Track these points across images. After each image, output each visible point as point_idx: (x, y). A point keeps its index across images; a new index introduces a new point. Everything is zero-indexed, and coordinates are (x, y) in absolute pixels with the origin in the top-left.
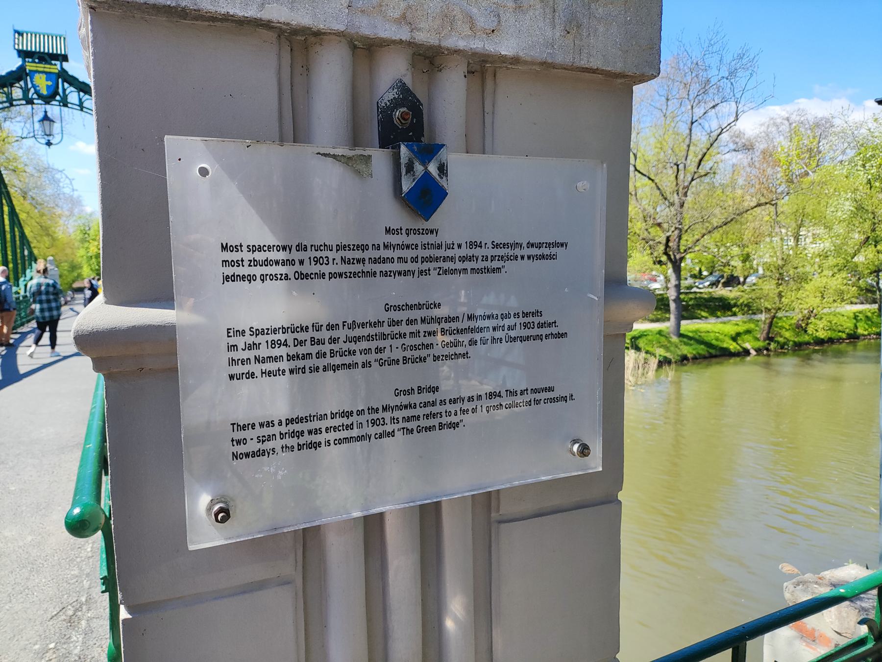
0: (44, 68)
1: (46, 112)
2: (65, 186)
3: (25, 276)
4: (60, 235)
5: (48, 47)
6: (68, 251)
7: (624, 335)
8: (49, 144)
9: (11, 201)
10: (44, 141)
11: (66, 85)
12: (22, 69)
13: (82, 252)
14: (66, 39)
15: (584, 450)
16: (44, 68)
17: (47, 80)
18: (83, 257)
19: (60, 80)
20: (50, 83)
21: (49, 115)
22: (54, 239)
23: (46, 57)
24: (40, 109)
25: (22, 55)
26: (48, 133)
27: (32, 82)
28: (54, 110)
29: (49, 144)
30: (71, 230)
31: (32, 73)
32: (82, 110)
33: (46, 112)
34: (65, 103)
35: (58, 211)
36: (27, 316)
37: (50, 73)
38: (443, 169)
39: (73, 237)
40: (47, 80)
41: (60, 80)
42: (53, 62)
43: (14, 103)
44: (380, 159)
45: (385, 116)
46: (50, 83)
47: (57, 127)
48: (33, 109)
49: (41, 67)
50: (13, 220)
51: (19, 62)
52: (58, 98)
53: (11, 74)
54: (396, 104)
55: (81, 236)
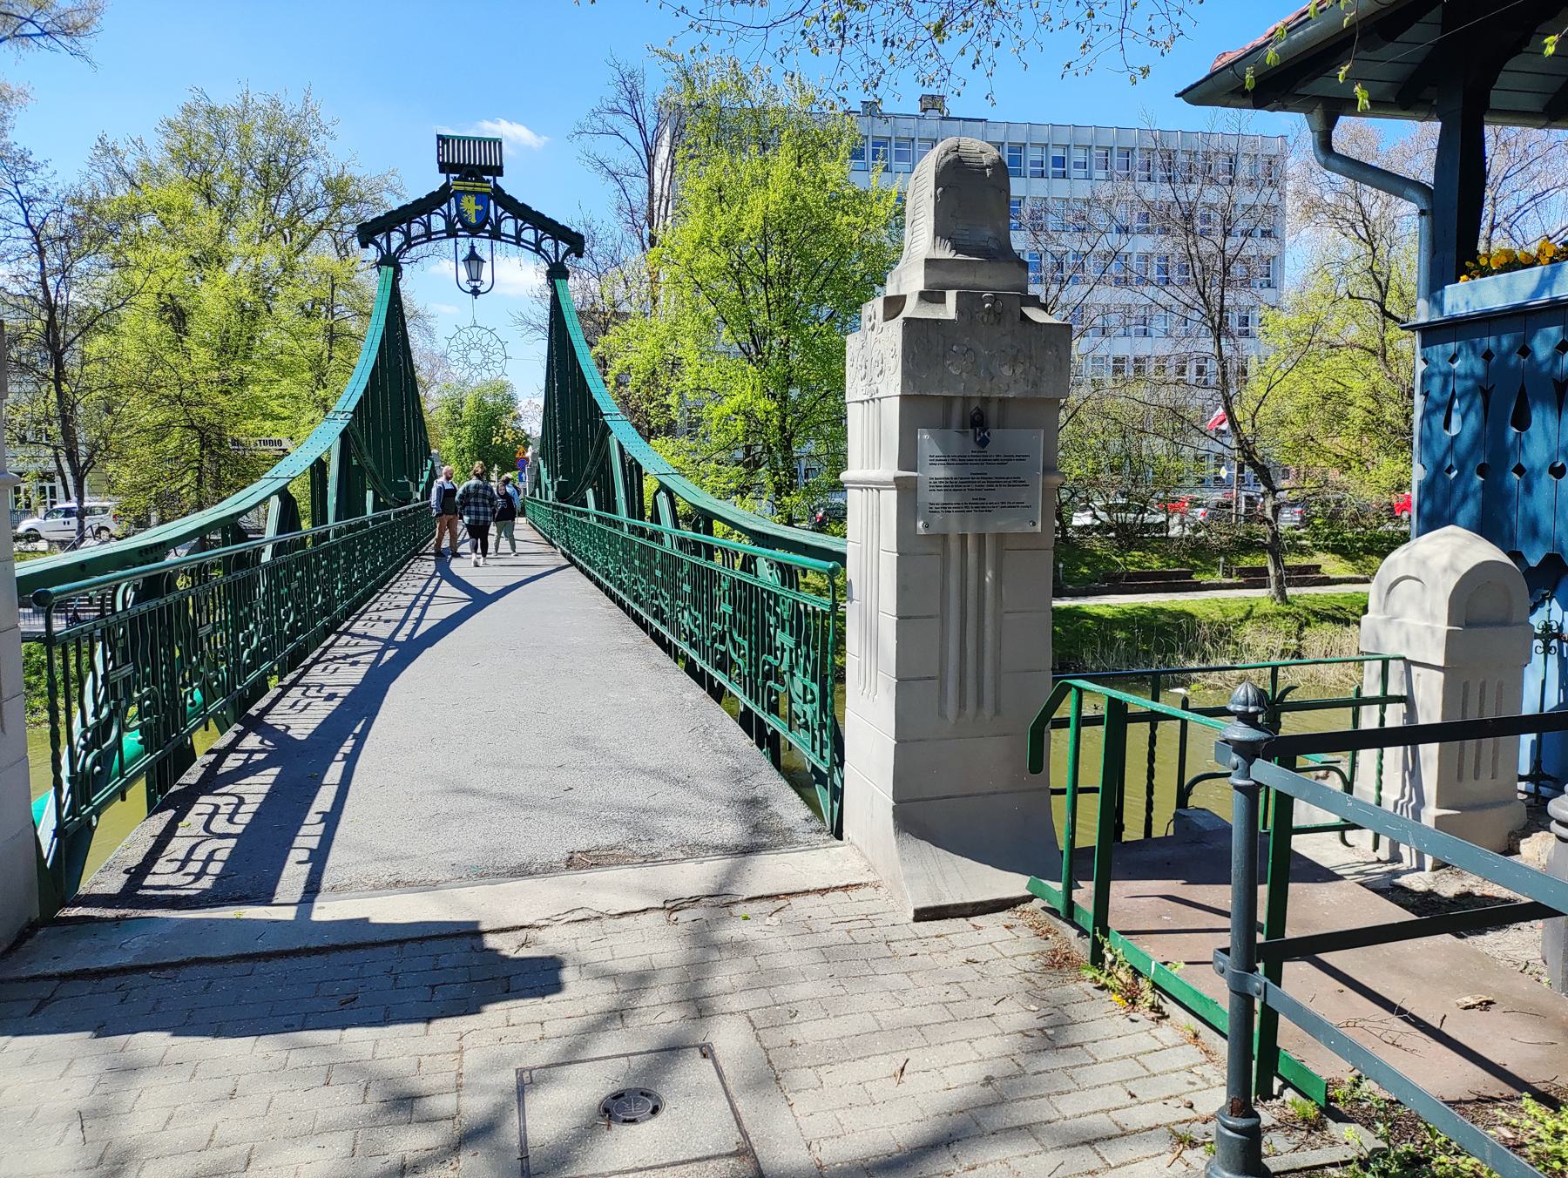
0: (475, 186)
1: (473, 247)
5: (477, 159)
8: (475, 292)
10: (469, 289)
11: (500, 210)
12: (446, 187)
14: (503, 144)
15: (1034, 524)
16: (475, 186)
18: (449, 449)
19: (492, 202)
21: (477, 251)
23: (477, 172)
24: (464, 244)
25: (447, 168)
26: (475, 277)
27: (458, 206)
28: (483, 246)
29: (475, 292)
31: (458, 194)
32: (518, 244)
33: (473, 247)
34: (496, 235)
37: (481, 193)
38: (989, 434)
41: (492, 202)
42: (486, 177)
43: (433, 237)
44: (971, 431)
45: (972, 418)
46: (480, 208)
48: (456, 243)
49: (469, 185)
51: (442, 179)
52: (488, 227)
53: (431, 196)
54: (976, 414)
55: (448, 416)
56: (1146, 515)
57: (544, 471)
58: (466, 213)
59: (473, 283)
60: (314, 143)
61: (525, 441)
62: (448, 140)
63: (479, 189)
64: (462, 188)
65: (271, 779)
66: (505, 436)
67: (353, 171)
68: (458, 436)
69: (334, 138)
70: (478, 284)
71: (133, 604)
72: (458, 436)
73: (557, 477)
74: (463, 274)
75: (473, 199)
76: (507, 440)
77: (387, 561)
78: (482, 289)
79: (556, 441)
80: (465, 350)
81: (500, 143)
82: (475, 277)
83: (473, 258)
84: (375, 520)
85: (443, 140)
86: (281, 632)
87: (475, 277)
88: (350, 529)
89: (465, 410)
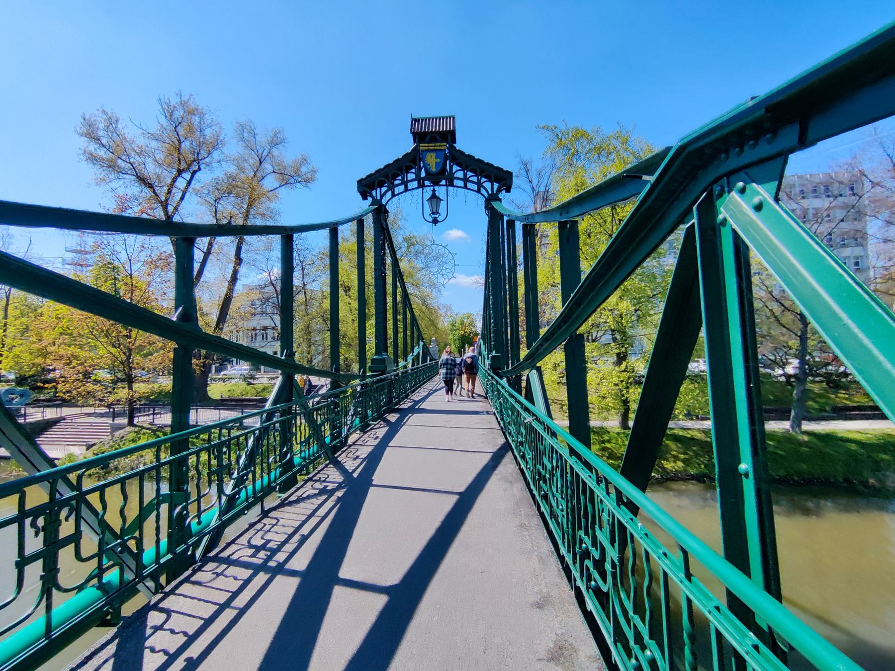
1: (434, 191)
2: (448, 261)
3: (413, 352)
4: (440, 326)
6: (444, 336)
7: (372, 363)
8: (435, 221)
9: (402, 279)
10: (430, 219)
13: (451, 336)
14: (456, 118)
17: (436, 158)
20: (438, 160)
21: (437, 193)
22: (437, 328)
26: (435, 211)
29: (435, 221)
30: (446, 324)
33: (434, 191)
34: (450, 183)
35: (440, 312)
36: (412, 387)
39: (447, 328)
40: (436, 158)
47: (443, 205)
50: (406, 302)
56: (276, 335)
57: (483, 347)
58: (429, 165)
59: (433, 216)
60: (400, 223)
61: (477, 335)
62: (419, 120)
63: (438, 148)
64: (427, 148)
65: (582, 278)
66: (466, 330)
67: (415, 234)
68: (454, 334)
69: (407, 221)
70: (437, 216)
71: (275, 402)
72: (454, 334)
73: (491, 352)
74: (428, 211)
75: (434, 155)
76: (466, 332)
77: (424, 379)
78: (439, 219)
79: (490, 334)
80: (434, 274)
81: (454, 118)
82: (435, 212)
83: (434, 197)
84: (421, 367)
85: (415, 121)
86: (381, 404)
87: (435, 212)
88: (424, 366)
89: (457, 325)
